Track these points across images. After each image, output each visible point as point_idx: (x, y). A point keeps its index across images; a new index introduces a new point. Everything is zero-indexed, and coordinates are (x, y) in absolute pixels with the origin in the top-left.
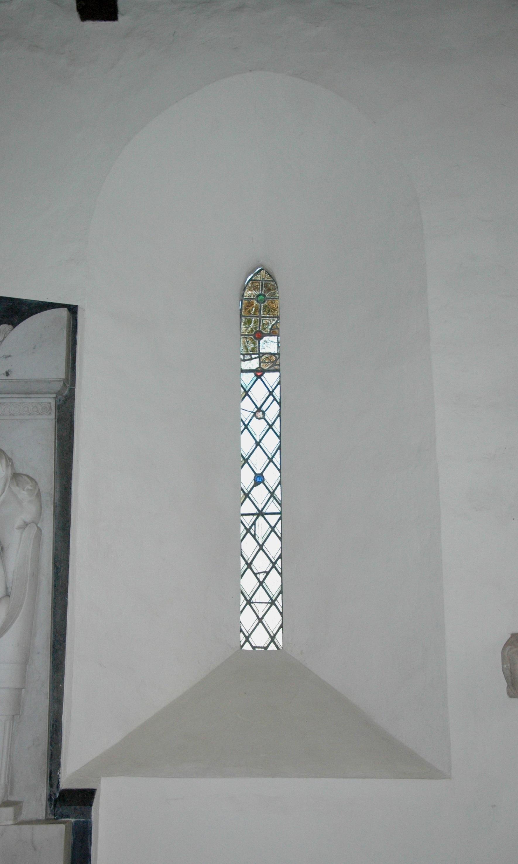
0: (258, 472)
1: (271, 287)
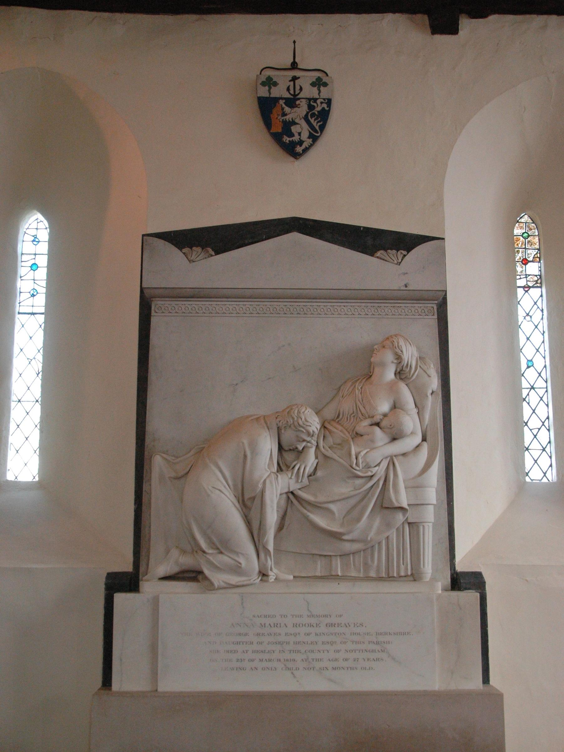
0: (530, 359)
1: (532, 228)
